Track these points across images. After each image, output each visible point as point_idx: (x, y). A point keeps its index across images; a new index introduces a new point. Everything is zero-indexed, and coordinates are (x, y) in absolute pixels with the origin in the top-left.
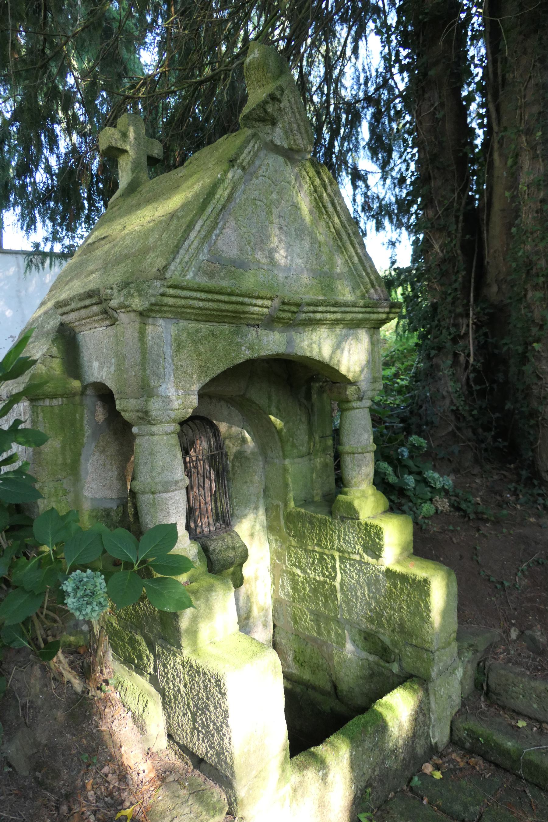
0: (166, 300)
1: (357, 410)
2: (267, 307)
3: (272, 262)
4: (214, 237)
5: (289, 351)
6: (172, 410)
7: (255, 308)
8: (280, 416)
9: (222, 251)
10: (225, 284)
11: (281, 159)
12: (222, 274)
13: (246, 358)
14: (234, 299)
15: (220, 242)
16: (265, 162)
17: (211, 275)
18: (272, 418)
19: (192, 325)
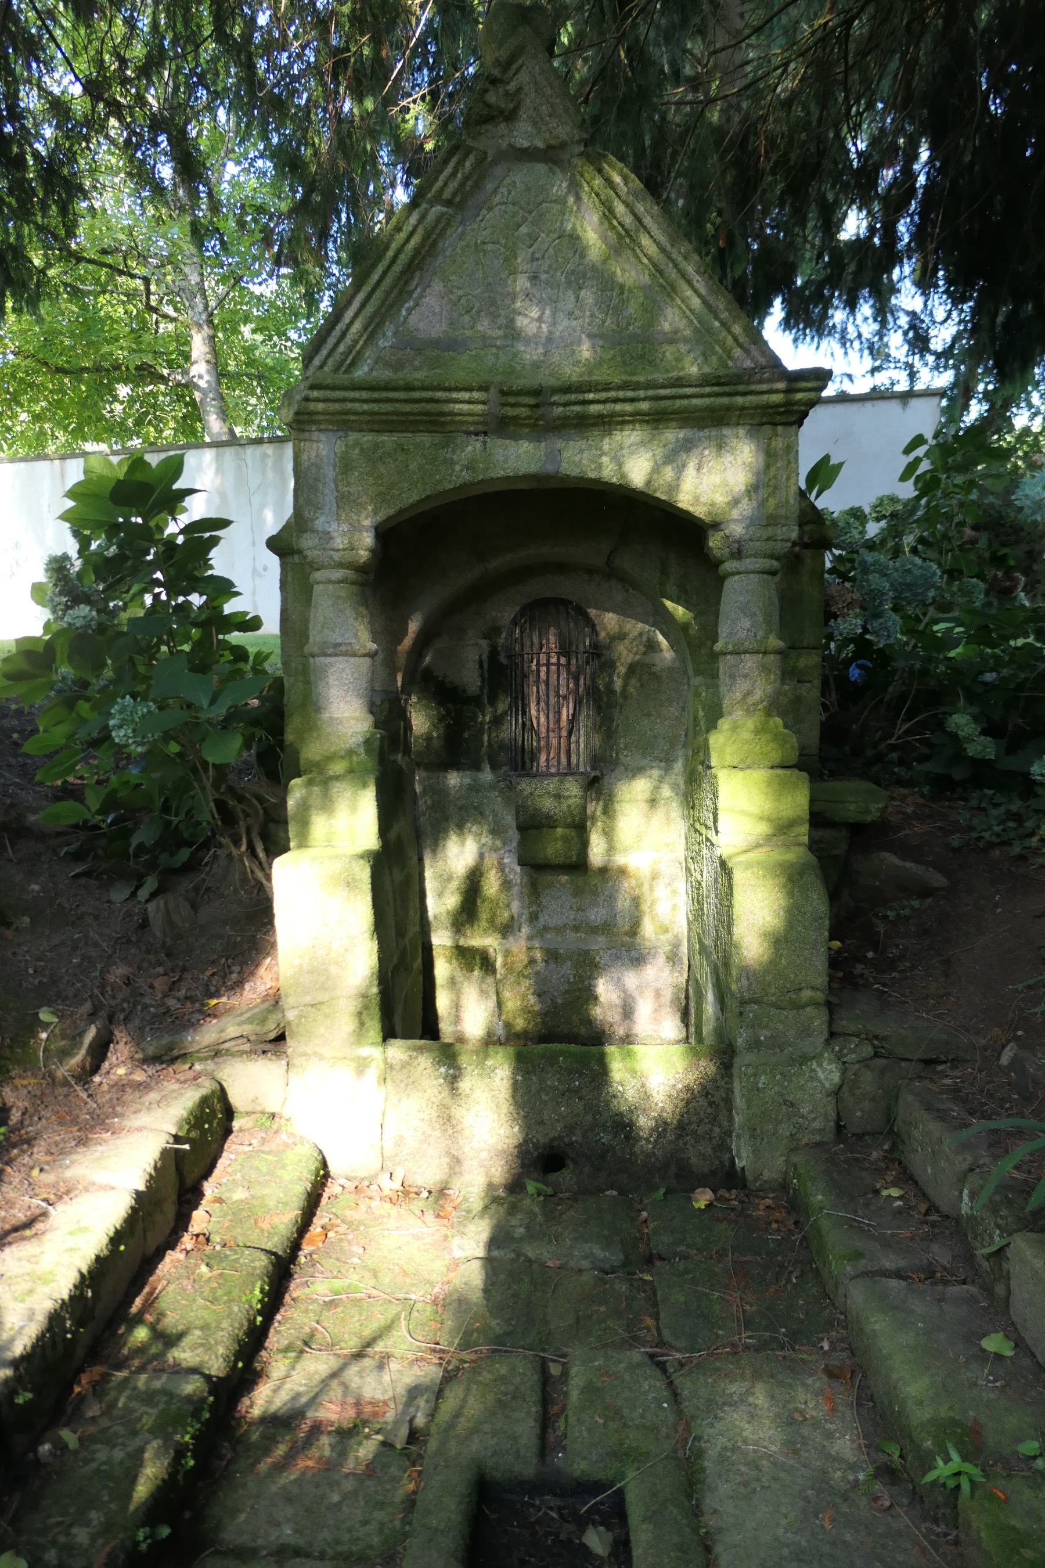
0: (312, 406)
1: (736, 578)
2: (483, 403)
3: (513, 334)
4: (404, 313)
5: (550, 468)
6: (333, 550)
7: (461, 406)
8: (687, 602)
9: (417, 330)
10: (419, 376)
11: (541, 168)
12: (416, 363)
13: (460, 481)
14: (416, 395)
15: (413, 319)
16: (508, 180)
17: (398, 366)
18: (668, 604)
19: (367, 439)
